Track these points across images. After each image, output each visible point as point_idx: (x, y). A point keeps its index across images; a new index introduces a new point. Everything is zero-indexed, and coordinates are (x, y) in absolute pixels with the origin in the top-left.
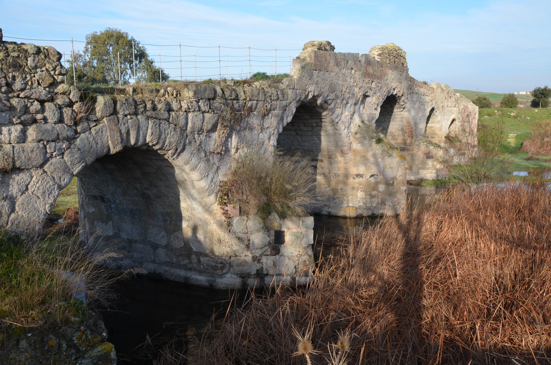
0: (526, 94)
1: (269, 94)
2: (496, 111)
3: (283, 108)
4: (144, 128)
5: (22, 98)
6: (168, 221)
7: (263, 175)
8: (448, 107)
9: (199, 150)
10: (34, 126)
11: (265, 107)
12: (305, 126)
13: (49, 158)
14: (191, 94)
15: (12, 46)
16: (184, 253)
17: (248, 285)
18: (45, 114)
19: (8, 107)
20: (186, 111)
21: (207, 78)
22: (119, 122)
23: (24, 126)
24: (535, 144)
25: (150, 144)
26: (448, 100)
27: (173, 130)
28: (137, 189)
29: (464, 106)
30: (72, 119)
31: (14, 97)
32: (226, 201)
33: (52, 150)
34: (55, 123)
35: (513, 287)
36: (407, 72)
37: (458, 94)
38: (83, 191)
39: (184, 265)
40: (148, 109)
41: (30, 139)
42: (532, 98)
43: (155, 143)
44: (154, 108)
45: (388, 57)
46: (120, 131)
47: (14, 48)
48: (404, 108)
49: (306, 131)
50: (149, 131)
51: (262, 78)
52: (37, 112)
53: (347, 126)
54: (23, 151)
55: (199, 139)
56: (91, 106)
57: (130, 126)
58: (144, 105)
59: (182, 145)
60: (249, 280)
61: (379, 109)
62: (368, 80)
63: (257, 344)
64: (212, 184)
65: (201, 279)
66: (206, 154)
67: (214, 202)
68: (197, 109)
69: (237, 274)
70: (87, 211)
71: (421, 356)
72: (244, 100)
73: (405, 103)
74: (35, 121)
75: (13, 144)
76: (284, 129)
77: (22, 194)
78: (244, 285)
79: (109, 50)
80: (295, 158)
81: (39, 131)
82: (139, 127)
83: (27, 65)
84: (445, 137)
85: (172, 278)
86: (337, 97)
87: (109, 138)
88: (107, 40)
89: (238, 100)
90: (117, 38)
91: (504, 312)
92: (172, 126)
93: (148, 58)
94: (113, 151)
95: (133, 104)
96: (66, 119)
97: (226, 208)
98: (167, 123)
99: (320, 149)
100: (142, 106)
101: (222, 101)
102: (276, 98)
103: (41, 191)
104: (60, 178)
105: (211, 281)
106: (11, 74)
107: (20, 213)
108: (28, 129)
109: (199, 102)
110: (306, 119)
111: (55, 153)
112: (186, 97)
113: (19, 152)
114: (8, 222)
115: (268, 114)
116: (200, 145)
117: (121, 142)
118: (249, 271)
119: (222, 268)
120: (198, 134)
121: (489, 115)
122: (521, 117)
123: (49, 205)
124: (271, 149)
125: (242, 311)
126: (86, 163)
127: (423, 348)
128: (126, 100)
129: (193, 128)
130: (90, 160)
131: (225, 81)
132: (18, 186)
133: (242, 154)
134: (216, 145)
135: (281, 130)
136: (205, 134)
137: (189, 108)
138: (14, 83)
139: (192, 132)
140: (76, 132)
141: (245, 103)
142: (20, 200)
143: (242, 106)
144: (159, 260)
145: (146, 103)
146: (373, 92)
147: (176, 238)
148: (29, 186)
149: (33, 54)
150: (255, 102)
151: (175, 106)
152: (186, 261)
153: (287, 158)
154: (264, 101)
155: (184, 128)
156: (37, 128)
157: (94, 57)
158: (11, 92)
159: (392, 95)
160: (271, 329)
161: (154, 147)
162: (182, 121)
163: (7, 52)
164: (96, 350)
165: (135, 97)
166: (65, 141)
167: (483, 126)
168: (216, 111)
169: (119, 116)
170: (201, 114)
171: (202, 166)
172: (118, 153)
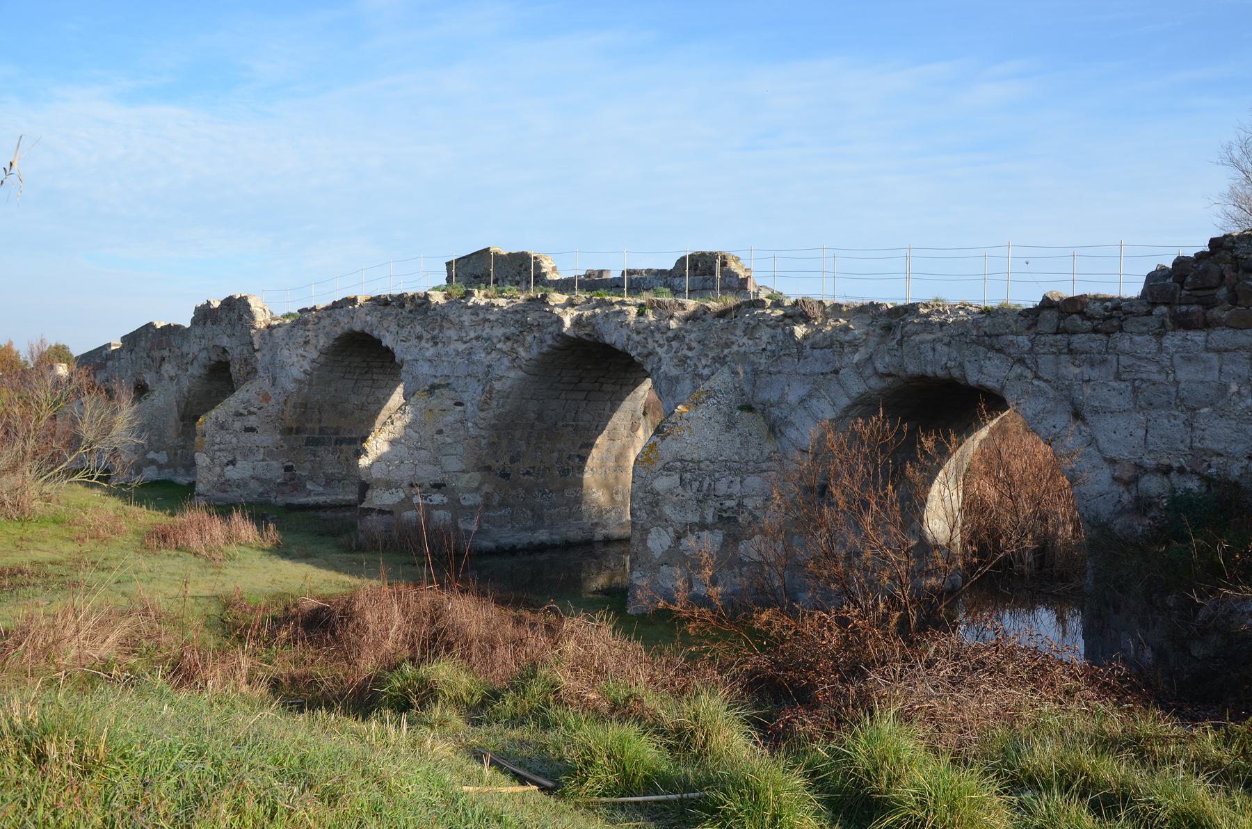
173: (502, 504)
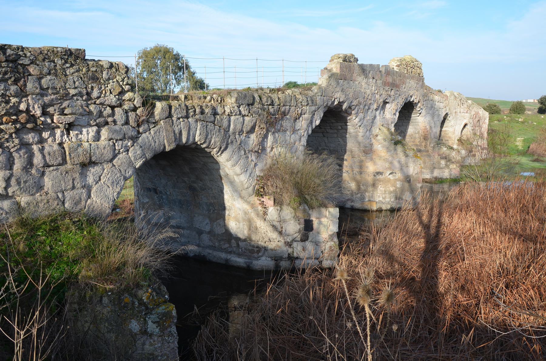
0: (534, 102)
1: (300, 100)
2: (505, 117)
3: (312, 112)
4: (194, 129)
5: (98, 104)
6: (212, 210)
7: (295, 171)
8: (460, 112)
9: (239, 148)
10: (106, 127)
11: (296, 111)
12: (331, 129)
13: (117, 154)
14: (233, 100)
15: (92, 63)
16: (225, 238)
17: (280, 267)
18: (115, 118)
19: (87, 112)
20: (228, 115)
21: (246, 87)
22: (173, 124)
23: (98, 127)
24: (541, 147)
25: (199, 143)
26: (461, 107)
27: (218, 131)
28: (185, 182)
29: (476, 112)
30: (135, 121)
31: (92, 103)
32: (262, 194)
33: (120, 148)
34: (122, 125)
35: (515, 270)
36: (423, 81)
37: (470, 102)
38: (138, 184)
39: (225, 249)
40: (197, 113)
41: (103, 138)
42: (539, 105)
43: (202, 142)
44: (202, 112)
45: (406, 68)
46: (174, 131)
47: (93, 64)
48: (420, 114)
50: (198, 132)
51: (294, 86)
52: (109, 116)
53: (369, 129)
54: (98, 148)
55: (240, 139)
56: (151, 110)
57: (182, 127)
58: (194, 109)
59: (225, 144)
60: (281, 262)
61: (398, 114)
62: (388, 88)
63: (289, 315)
64: (250, 178)
65: (240, 261)
66: (245, 152)
67: (252, 194)
68: (238, 113)
69: (271, 257)
70: (142, 201)
71: (431, 327)
72: (278, 105)
73: (422, 109)
74: (107, 123)
75: (90, 142)
76: (313, 131)
77: (96, 184)
78: (277, 266)
79: (157, 63)
80: (324, 156)
81: (112, 131)
82: (189, 128)
83: (102, 77)
84: (458, 140)
85: (214, 260)
86: (360, 103)
87: (165, 137)
88: (156, 55)
89: (273, 105)
90: (164, 52)
91: (505, 290)
92: (217, 127)
93: (191, 69)
94: (168, 149)
95: (185, 109)
96: (131, 121)
97: (262, 199)
98: (213, 125)
100: (192, 110)
101: (260, 106)
102: (306, 104)
103: (110, 181)
104: (126, 171)
105: (248, 262)
106: (90, 85)
107: (94, 199)
108: (101, 130)
109: (240, 107)
110: (332, 123)
111: (122, 150)
112: (229, 103)
113: (94, 149)
114: (85, 207)
115: (299, 118)
116: (240, 144)
117: (175, 141)
118: (282, 255)
119: (258, 252)
120: (239, 135)
121: (499, 121)
122: (528, 123)
123: (117, 193)
124: (301, 148)
125: (277, 287)
126: (146, 158)
127: (434, 320)
128: (179, 105)
129: (234, 129)
130: (149, 155)
131: (262, 89)
132: (93, 177)
133: (276, 153)
134: (254, 145)
135: (310, 132)
136: (245, 135)
137: (231, 113)
138: (92, 92)
139: (234, 133)
140: (139, 132)
141: (280, 108)
142: (94, 188)
143: (277, 111)
144: (203, 244)
145: (196, 107)
146: (392, 99)
147: (218, 225)
148: (102, 177)
149: (107, 68)
150: (288, 107)
151: (219, 110)
152: (227, 245)
153: (315, 156)
154: (296, 106)
155: (227, 130)
156: (108, 129)
157: (144, 69)
158: (89, 100)
159: (409, 101)
160: (302, 303)
161: (201, 146)
162: (225, 124)
163: (88, 68)
164: (161, 308)
165: (186, 102)
166: (130, 140)
167: (493, 130)
168: (254, 115)
169: (173, 119)
170: (242, 118)
171: (242, 162)
172: (171, 151)
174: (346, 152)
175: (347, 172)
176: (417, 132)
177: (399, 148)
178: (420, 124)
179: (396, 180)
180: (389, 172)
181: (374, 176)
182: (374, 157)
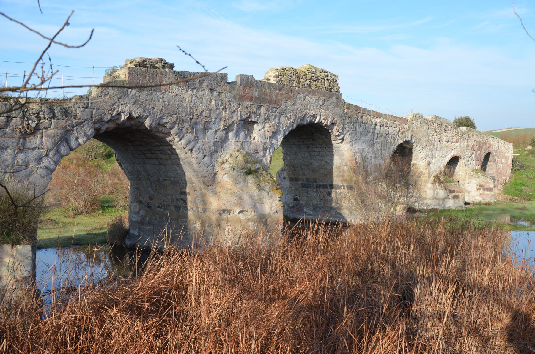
49: (165, 159)
99: (185, 180)
173: (150, 223)
174: (186, 184)
175: (192, 209)
176: (344, 163)
177: (251, 179)
178: (345, 153)
179: (248, 220)
180: (238, 210)
181: (220, 214)
182: (218, 190)
